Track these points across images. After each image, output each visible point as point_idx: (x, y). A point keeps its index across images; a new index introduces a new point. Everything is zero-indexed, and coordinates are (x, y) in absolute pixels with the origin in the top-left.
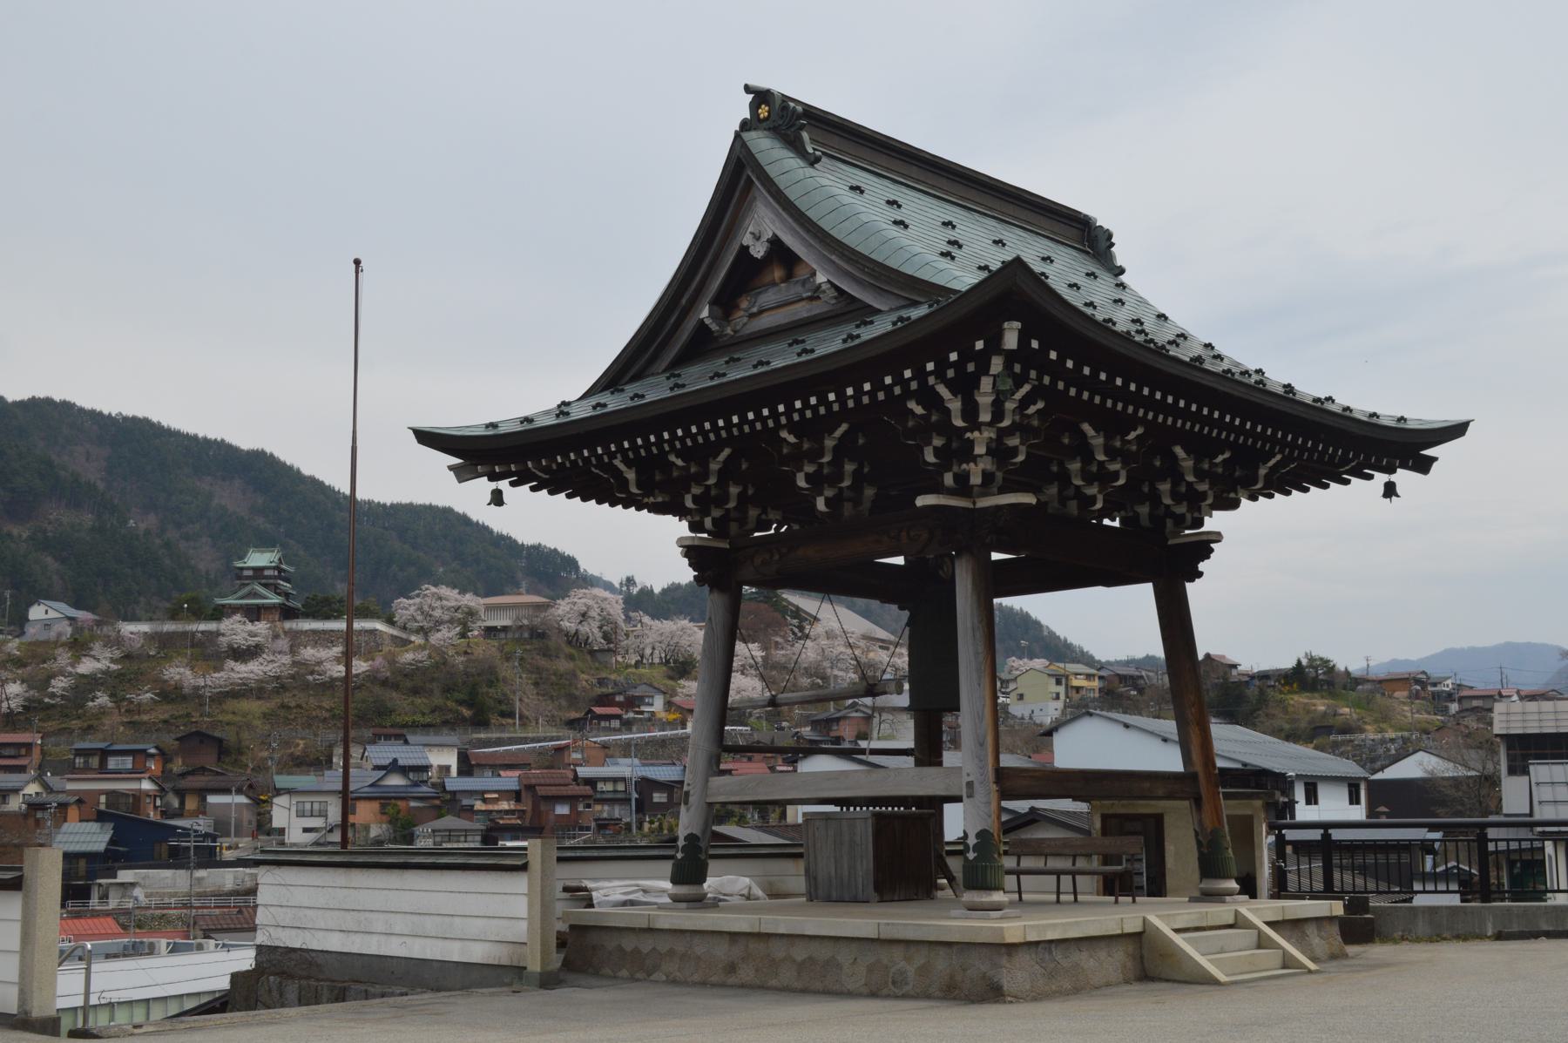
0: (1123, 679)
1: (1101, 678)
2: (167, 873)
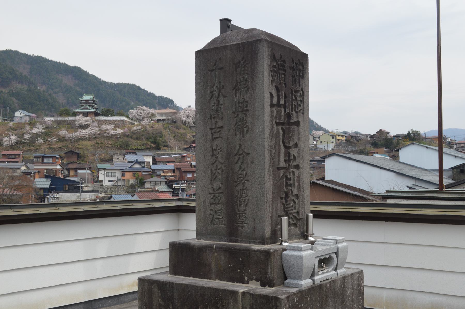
0: (352, 137)
1: (346, 136)
2: (68, 195)
